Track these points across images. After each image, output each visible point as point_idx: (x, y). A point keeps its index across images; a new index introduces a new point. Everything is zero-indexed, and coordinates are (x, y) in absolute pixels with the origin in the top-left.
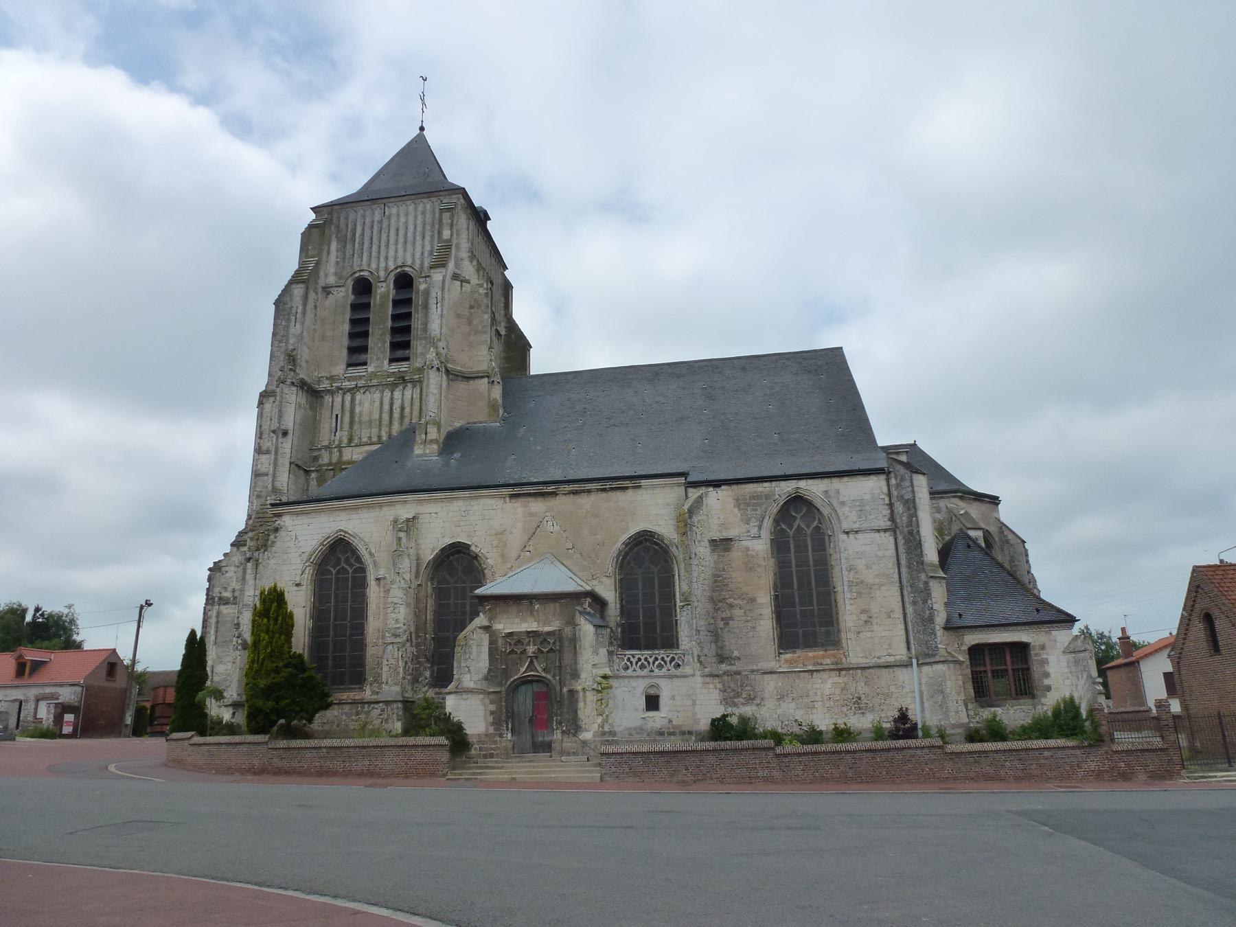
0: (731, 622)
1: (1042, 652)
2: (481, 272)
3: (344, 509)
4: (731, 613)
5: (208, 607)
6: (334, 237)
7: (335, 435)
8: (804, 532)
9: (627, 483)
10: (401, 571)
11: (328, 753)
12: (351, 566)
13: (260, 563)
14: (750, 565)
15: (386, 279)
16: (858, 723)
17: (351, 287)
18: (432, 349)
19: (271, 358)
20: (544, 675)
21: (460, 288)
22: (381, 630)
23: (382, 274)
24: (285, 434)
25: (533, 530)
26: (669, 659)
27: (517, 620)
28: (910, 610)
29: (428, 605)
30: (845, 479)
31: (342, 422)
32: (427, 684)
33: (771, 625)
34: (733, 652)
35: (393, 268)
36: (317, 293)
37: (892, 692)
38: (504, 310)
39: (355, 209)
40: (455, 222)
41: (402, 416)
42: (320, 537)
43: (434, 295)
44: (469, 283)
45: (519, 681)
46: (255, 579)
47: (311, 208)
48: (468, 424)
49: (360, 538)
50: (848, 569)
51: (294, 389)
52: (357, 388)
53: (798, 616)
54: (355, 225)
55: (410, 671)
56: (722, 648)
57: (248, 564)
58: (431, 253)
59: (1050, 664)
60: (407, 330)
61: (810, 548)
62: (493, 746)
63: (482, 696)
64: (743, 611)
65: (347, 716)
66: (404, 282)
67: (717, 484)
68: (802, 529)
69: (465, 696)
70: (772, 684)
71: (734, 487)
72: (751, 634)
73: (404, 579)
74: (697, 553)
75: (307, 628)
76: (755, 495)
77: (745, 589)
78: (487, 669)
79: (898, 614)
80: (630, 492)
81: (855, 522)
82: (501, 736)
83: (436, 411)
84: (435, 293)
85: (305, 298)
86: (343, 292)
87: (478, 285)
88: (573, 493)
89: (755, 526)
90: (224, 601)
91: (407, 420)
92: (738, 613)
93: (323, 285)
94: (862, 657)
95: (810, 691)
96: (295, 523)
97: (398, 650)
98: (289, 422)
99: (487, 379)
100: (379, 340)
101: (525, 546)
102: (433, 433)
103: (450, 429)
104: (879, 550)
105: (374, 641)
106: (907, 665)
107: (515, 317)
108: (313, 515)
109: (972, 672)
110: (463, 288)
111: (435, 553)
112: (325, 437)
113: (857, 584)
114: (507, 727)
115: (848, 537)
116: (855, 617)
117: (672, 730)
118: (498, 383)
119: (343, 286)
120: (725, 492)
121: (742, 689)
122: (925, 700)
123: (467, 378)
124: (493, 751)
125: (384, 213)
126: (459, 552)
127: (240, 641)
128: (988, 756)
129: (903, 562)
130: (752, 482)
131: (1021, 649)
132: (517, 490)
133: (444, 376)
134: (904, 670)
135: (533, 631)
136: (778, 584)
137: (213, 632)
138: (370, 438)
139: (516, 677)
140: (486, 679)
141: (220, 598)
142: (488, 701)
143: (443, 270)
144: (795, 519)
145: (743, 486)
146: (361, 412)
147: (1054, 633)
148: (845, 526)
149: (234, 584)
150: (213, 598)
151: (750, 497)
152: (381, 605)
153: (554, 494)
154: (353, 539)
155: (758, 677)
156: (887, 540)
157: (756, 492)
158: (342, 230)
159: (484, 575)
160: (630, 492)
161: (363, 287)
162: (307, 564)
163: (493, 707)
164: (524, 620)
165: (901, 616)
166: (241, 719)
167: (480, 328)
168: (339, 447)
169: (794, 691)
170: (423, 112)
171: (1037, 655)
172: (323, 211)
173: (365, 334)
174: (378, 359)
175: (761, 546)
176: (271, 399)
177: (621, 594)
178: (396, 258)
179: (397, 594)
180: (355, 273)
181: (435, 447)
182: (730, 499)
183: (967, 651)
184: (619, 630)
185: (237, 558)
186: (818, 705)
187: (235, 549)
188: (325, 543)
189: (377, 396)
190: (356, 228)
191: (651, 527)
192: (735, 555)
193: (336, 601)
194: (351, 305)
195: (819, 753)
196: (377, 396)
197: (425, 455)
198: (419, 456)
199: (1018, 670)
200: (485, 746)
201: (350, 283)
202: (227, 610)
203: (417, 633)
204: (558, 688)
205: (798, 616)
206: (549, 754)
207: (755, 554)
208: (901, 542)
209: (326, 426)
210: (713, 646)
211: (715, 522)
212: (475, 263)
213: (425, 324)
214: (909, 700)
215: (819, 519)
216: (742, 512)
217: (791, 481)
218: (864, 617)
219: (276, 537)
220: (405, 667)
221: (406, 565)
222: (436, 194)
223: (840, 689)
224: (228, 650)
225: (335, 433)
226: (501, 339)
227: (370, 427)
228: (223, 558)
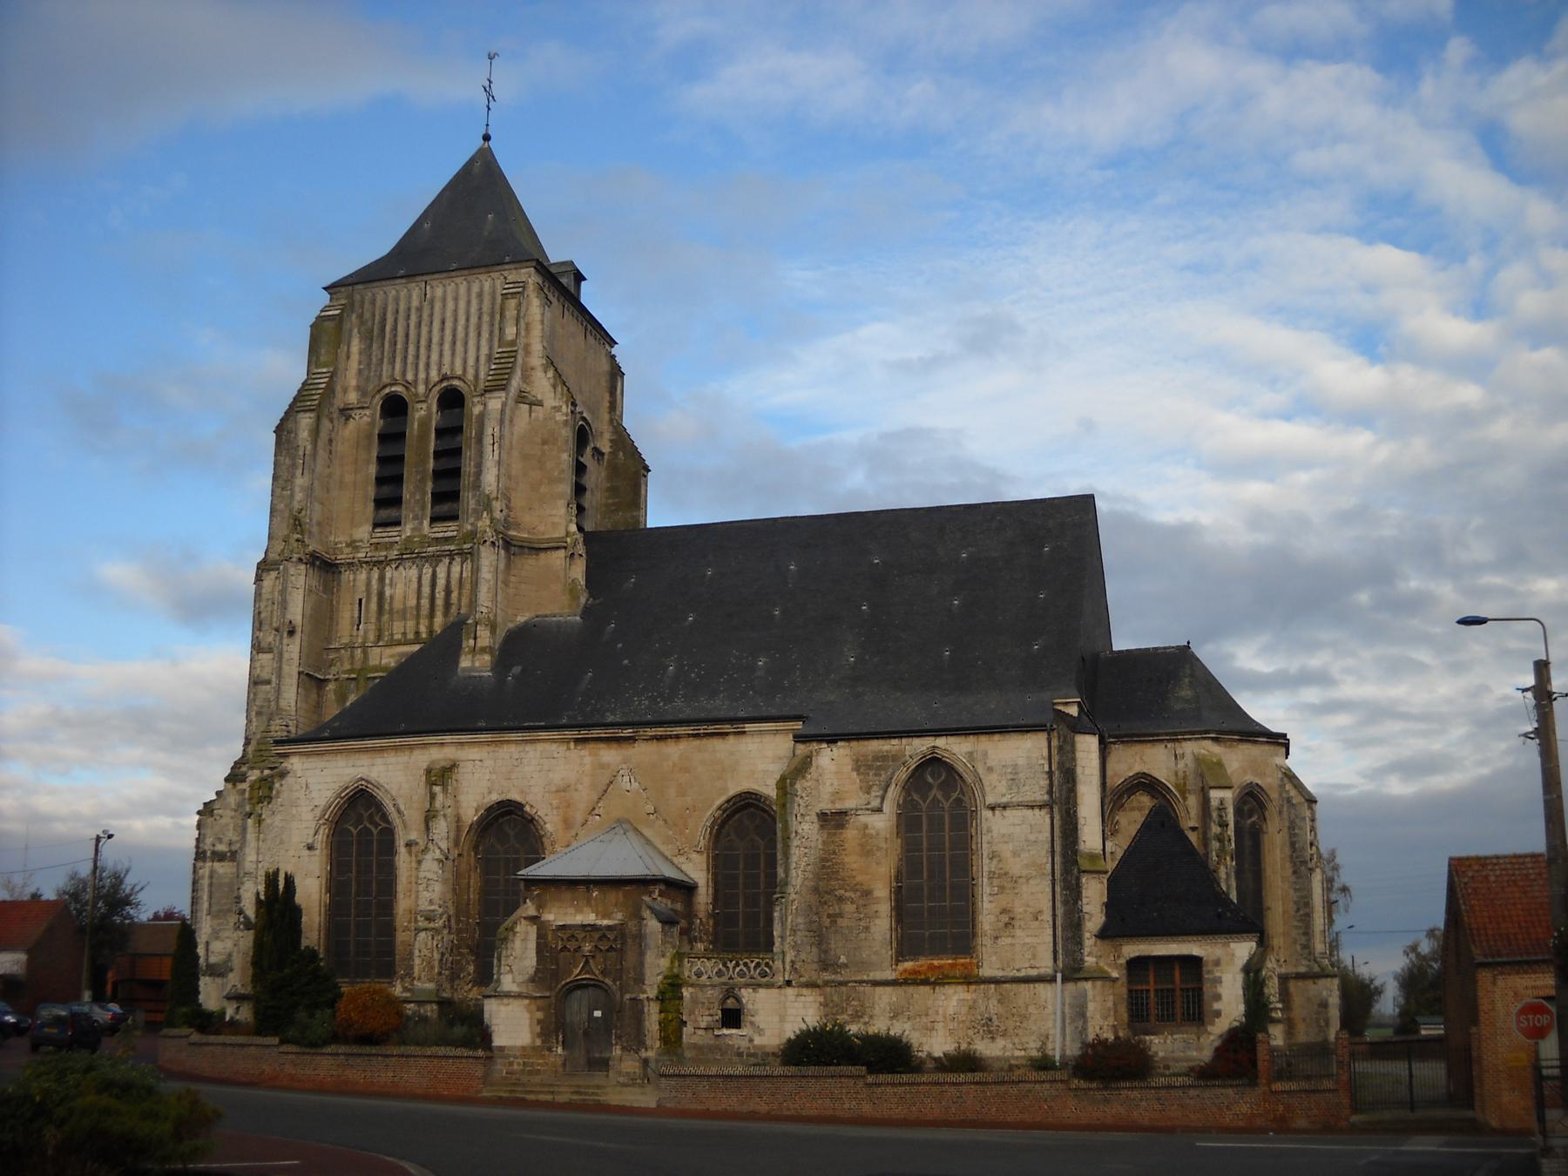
0: (839, 921)
1: (1216, 968)
2: (559, 389)
3: (366, 750)
4: (840, 908)
5: (200, 864)
6: (356, 330)
7: (358, 629)
8: (941, 805)
9: (727, 728)
10: (435, 837)
12: (376, 825)
13: (264, 820)
14: (868, 847)
15: (427, 397)
16: (986, 1049)
17: (379, 408)
18: (485, 514)
19: (271, 512)
20: (600, 978)
21: (528, 414)
22: (413, 912)
23: (421, 389)
24: (291, 633)
25: (604, 788)
26: (753, 964)
27: (572, 910)
28: (1060, 912)
29: (472, 881)
30: (997, 737)
32: (470, 982)
33: (888, 927)
34: (840, 957)
35: (437, 379)
36: (331, 420)
37: (1030, 1013)
38: (610, 413)
40: (522, 315)
41: (447, 604)
42: (336, 786)
43: (489, 431)
44: (542, 406)
45: (571, 985)
46: (258, 840)
47: (325, 288)
48: (537, 617)
49: (386, 791)
50: (991, 856)
51: (303, 567)
52: (388, 562)
53: (926, 914)
54: (385, 314)
55: (449, 965)
56: (826, 952)
57: (249, 820)
58: (489, 357)
59: (1223, 984)
60: (455, 473)
61: (947, 826)
62: (540, 1061)
63: (527, 1002)
64: (855, 906)
66: (452, 400)
67: (832, 740)
68: (939, 801)
69: (505, 1001)
70: (885, 999)
71: (854, 744)
72: (863, 935)
73: (439, 848)
74: (800, 831)
75: (322, 904)
76: (881, 754)
77: (859, 878)
78: (534, 969)
79: (1047, 916)
80: (731, 740)
81: (1003, 795)
82: (550, 1050)
83: (490, 604)
84: (491, 428)
85: (315, 432)
86: (368, 417)
87: (555, 407)
88: (657, 739)
89: (876, 796)
90: (219, 857)
91: (454, 610)
92: (849, 908)
93: (342, 406)
94: (998, 969)
95: (930, 1008)
96: (307, 765)
97: (433, 939)
98: (297, 610)
99: (564, 551)
100: (417, 489)
101: (594, 809)
102: (484, 637)
103: (511, 625)
104: (1031, 833)
105: (405, 924)
106: (1052, 980)
107: (627, 423)
109: (1130, 991)
110: (533, 415)
111: (480, 813)
112: (344, 630)
113: (1000, 876)
114: (557, 1039)
115: (994, 815)
116: (992, 918)
117: (752, 1051)
118: (581, 555)
119: (368, 408)
120: (841, 751)
121: (847, 1004)
122: (1067, 1024)
123: (535, 549)
124: (539, 1067)
125: (426, 295)
126: (509, 813)
127: (242, 920)
128: (1120, 1094)
129: (1058, 848)
130: (877, 738)
131: (1194, 963)
133: (502, 552)
134: (1048, 986)
135: (589, 925)
136: (904, 871)
137: (205, 897)
138: (404, 634)
139: (568, 981)
140: (532, 980)
141: (214, 853)
142: (534, 1007)
143: (503, 394)
144: (930, 787)
145: (866, 743)
146: (392, 597)
147: (1232, 945)
148: (990, 800)
149: (231, 835)
150: (204, 852)
151: (873, 757)
152: (414, 880)
153: (632, 740)
154: (377, 791)
155: (868, 989)
156: (1041, 818)
157: (881, 751)
158: (367, 321)
159: (542, 843)
160: (731, 739)
161: (395, 407)
162: (321, 822)
163: (540, 1015)
164: (579, 910)
165: (1050, 919)
166: (245, 1014)
167: (556, 474)
168: (364, 648)
169: (911, 1007)
170: (489, 109)
171: (1209, 972)
173: (398, 480)
174: (416, 518)
175: (882, 823)
176: (273, 574)
177: (715, 875)
178: (440, 365)
179: (430, 867)
180: (385, 387)
181: (487, 657)
182: (848, 760)
183: (1125, 965)
184: (711, 922)
185: (232, 799)
186: (939, 1026)
187: (230, 786)
188: (343, 795)
189: (414, 572)
190: (385, 319)
191: (756, 787)
192: (850, 834)
193: (358, 872)
194: (379, 435)
195: (919, 1084)
196: (414, 572)
197: (472, 669)
198: (464, 669)
199: (1188, 990)
200: (531, 1060)
201: (378, 402)
202: (223, 868)
203: (457, 916)
204: (618, 995)
205: (926, 914)
206: (605, 1073)
207: (874, 834)
208: (1057, 817)
209: (346, 614)
210: (814, 949)
211: (826, 790)
212: (551, 374)
213: (479, 473)
214: (1050, 1024)
215: (962, 789)
216: (862, 777)
217: (928, 738)
218: (1005, 918)
219: (281, 785)
220: (441, 960)
221: (441, 828)
223: (967, 1008)
224: (225, 922)
225: (358, 625)
226: (603, 459)
227: (404, 619)
228: (214, 797)
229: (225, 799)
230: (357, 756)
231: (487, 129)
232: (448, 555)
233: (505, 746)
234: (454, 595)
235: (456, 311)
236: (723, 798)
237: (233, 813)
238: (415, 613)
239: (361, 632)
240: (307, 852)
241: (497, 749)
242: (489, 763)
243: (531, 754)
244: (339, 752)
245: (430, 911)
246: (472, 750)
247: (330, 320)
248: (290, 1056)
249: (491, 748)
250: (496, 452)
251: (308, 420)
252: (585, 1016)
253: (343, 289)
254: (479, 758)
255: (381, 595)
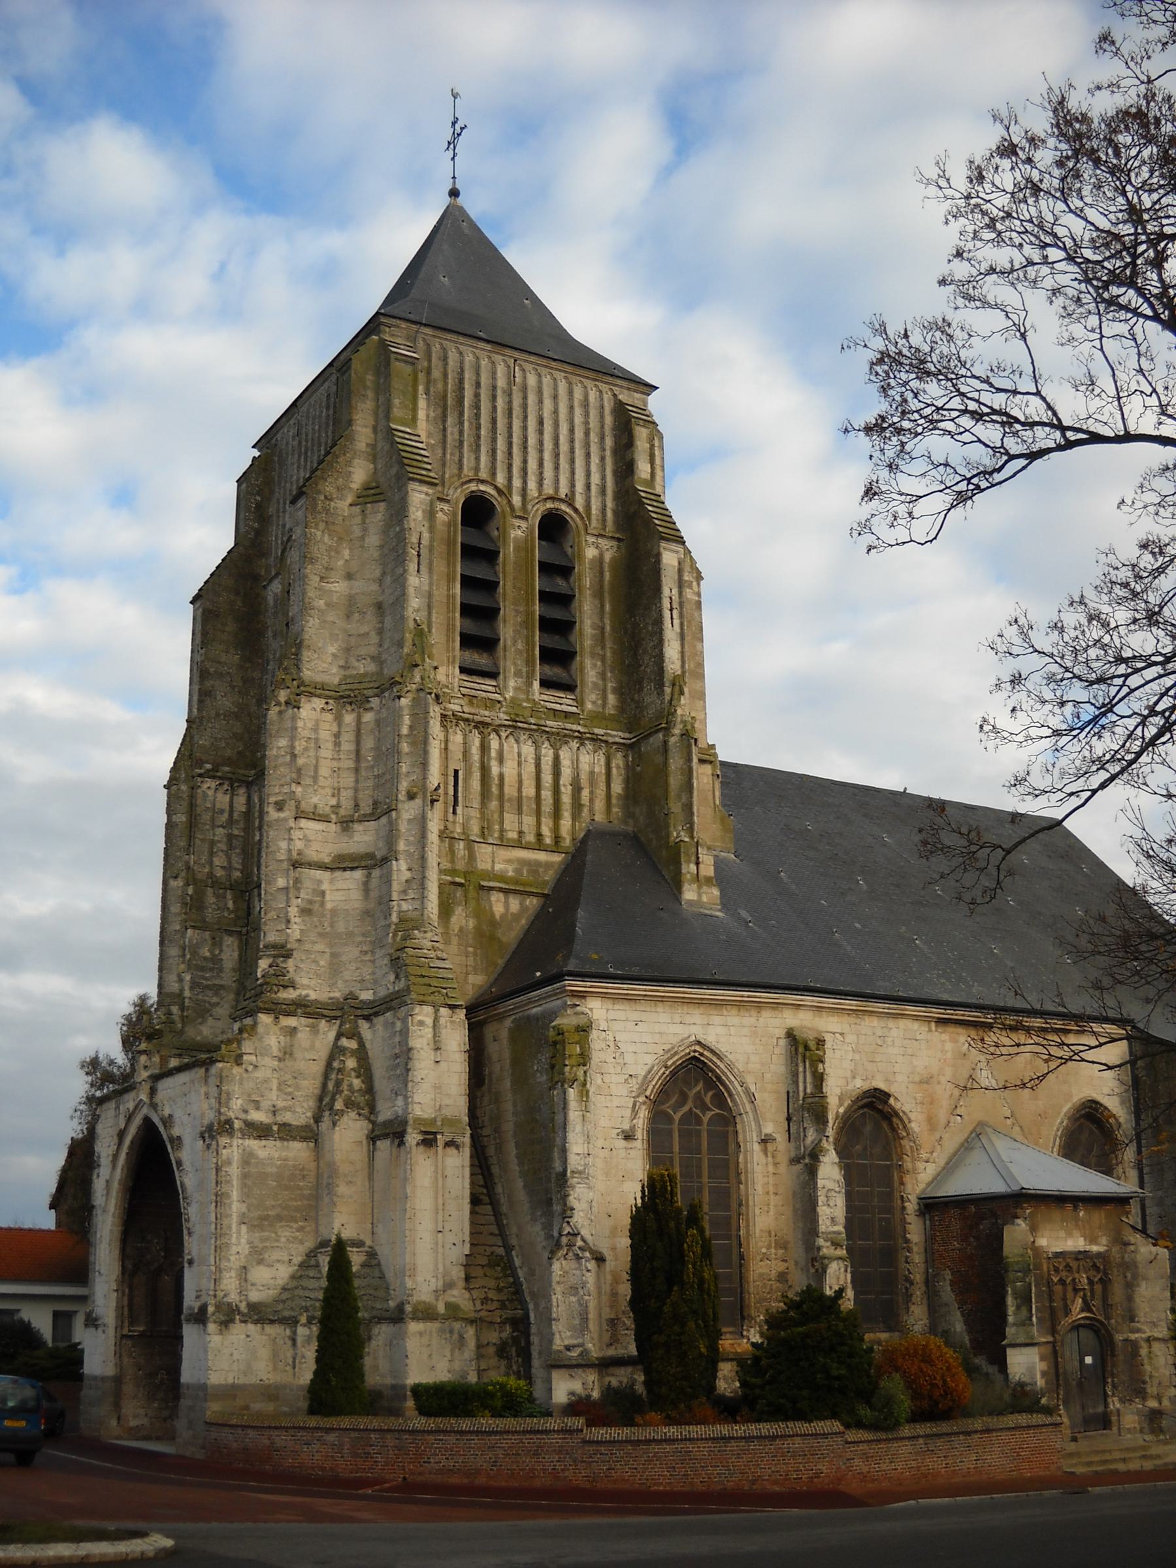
3: (700, 1003)
7: (454, 812)
11: (926, 1444)
22: (773, 1233)
27: (1062, 1234)
31: (466, 788)
39: (462, 348)
41: (577, 805)
65: (727, 1383)
86: (445, 514)
91: (585, 812)
96: (612, 1015)
105: (764, 1250)
108: (641, 1006)
111: (846, 1104)
132: (949, 1014)
141: (249, 1124)
172: (397, 327)
188: (669, 1063)
195: (546, 1432)
198: (690, 902)
222: (611, 379)
229: (260, 1040)
230: (686, 1008)
231: (454, 182)
232: (577, 737)
233: (866, 1018)
234: (585, 793)
235: (556, 412)
236: (1069, 1105)
237: (276, 1063)
238: (534, 806)
239: (460, 818)
240: (622, 1143)
241: (858, 1021)
242: (850, 1038)
243: (894, 1032)
244: (662, 1000)
245: (834, 1233)
246: (831, 1019)
247: (405, 362)
248: (862, 1447)
249: (852, 1020)
250: (676, 622)
251: (423, 496)
252: (1077, 1364)
253: (404, 325)
254: (840, 1031)
255: (485, 770)
